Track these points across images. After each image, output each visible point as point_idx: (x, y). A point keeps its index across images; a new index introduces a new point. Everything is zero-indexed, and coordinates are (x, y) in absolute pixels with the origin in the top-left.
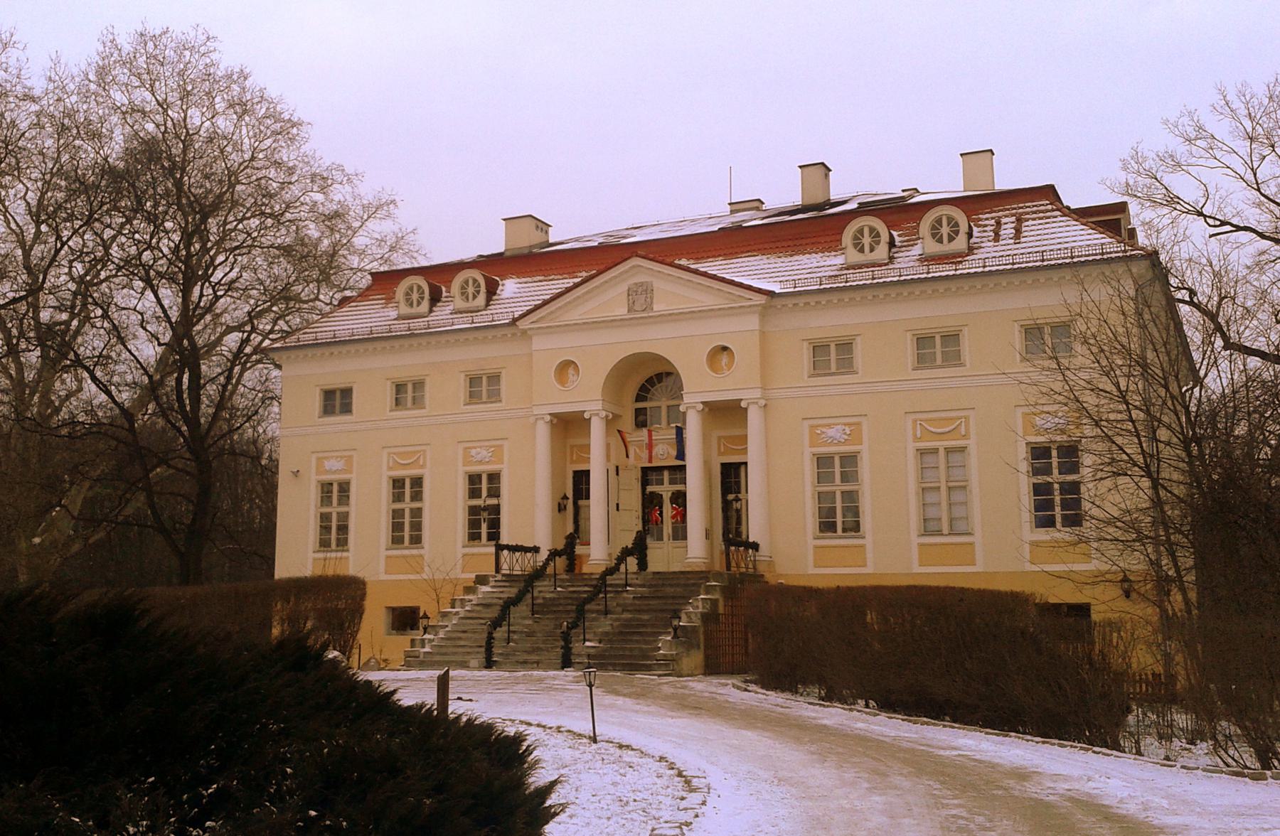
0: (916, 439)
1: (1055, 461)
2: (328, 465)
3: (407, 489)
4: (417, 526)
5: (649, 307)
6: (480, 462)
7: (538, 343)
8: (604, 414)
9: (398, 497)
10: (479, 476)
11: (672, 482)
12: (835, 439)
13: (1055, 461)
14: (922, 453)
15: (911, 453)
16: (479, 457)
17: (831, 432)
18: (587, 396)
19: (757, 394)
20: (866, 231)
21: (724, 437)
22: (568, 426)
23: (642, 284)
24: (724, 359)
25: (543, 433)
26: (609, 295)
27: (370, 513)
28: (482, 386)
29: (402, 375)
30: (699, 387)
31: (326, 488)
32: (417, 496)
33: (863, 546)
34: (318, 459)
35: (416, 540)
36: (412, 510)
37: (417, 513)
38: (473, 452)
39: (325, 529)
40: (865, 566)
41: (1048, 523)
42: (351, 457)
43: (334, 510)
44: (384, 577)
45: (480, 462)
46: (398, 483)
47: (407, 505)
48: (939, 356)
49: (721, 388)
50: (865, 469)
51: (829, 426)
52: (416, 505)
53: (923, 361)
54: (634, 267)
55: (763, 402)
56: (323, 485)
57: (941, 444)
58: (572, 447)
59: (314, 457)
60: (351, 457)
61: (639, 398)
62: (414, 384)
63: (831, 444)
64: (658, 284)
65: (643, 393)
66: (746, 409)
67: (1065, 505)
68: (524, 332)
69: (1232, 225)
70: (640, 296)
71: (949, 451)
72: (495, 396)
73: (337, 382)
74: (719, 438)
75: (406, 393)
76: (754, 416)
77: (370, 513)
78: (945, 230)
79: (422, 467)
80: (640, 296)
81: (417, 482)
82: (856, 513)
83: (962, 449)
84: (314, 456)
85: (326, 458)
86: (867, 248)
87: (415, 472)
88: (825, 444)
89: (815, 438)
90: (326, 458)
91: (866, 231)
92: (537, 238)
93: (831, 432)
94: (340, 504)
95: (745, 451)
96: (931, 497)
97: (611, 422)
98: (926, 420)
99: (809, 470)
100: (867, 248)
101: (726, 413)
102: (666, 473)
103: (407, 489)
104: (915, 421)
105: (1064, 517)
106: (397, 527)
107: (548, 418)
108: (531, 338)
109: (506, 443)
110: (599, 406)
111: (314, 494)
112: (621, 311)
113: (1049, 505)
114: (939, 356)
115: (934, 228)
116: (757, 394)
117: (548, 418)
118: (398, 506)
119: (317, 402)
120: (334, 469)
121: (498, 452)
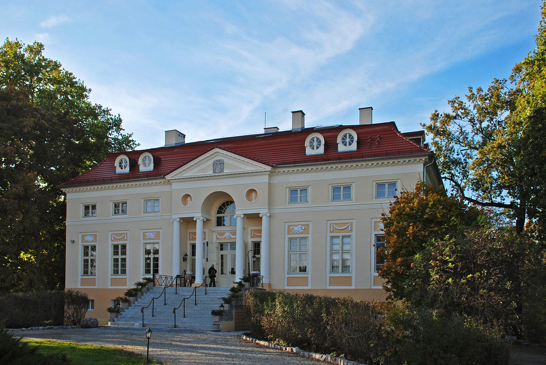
0: (112, 241)
2: (86, 238)
3: (120, 249)
4: (124, 266)
5: (222, 171)
7: (175, 186)
8: (202, 218)
9: (116, 253)
10: (88, 247)
14: (332, 237)
16: (149, 237)
19: (266, 211)
20: (315, 139)
21: (254, 230)
22: (188, 222)
24: (253, 195)
25: (176, 226)
26: (202, 166)
27: (104, 258)
32: (124, 253)
34: (144, 233)
36: (88, 260)
37: (124, 260)
38: (147, 234)
39: (116, 266)
42: (96, 235)
43: (120, 257)
44: (110, 287)
46: (116, 247)
48: (299, 198)
52: (123, 257)
55: (268, 215)
56: (114, 246)
57: (341, 234)
58: (190, 233)
60: (96, 235)
61: (219, 212)
62: (92, 206)
63: (296, 234)
64: (226, 161)
65: (221, 210)
66: (262, 217)
68: (169, 181)
70: (219, 165)
71: (301, 238)
72: (348, 197)
73: (90, 202)
74: (251, 230)
75: (119, 207)
76: (265, 220)
77: (104, 258)
78: (348, 140)
79: (126, 240)
81: (124, 247)
83: (306, 238)
86: (315, 148)
88: (294, 233)
89: (290, 231)
91: (315, 139)
92: (180, 141)
93: (296, 228)
94: (122, 254)
95: (261, 236)
97: (206, 222)
98: (335, 224)
100: (315, 148)
103: (120, 249)
104: (331, 224)
107: (179, 219)
108: (172, 183)
109: (354, 221)
110: (200, 215)
112: (210, 173)
114: (299, 198)
115: (343, 139)
117: (179, 219)
118: (116, 257)
120: (89, 240)
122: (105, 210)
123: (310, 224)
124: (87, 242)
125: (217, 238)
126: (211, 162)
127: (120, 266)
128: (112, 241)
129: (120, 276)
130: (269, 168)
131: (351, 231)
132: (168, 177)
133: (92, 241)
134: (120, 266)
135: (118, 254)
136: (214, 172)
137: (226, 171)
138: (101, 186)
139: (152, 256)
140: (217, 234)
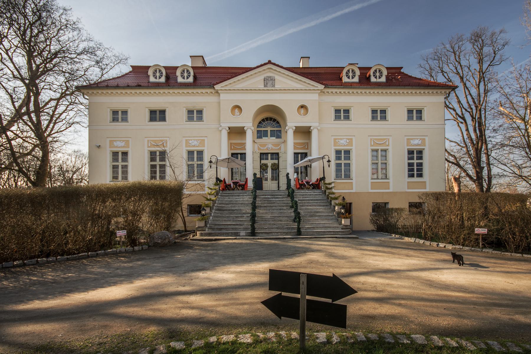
0: (148, 147)
1: (415, 155)
5: (274, 86)
6: (194, 146)
11: (272, 159)
12: (415, 144)
13: (415, 155)
15: (370, 151)
16: (193, 144)
17: (342, 142)
18: (247, 121)
22: (237, 132)
23: (270, 77)
25: (225, 134)
27: (398, 163)
28: (195, 114)
29: (116, 107)
30: (293, 120)
31: (115, 154)
32: (421, 158)
33: (352, 183)
34: (111, 141)
35: (420, 175)
38: (190, 142)
40: (352, 189)
41: (412, 176)
45: (194, 146)
47: (343, 162)
49: (303, 121)
50: (353, 155)
51: (341, 139)
53: (374, 118)
54: (268, 68)
57: (380, 148)
59: (108, 140)
60: (128, 141)
64: (277, 77)
67: (418, 170)
69: (480, 82)
70: (269, 81)
75: (158, 115)
79: (388, 145)
80: (269, 81)
82: (113, 172)
84: (108, 140)
85: (115, 141)
87: (199, 149)
88: (339, 146)
90: (115, 141)
93: (342, 142)
96: (384, 166)
99: (185, 156)
101: (304, 132)
102: (239, 155)
105: (417, 174)
106: (411, 170)
107: (228, 129)
110: (251, 124)
111: (109, 157)
112: (262, 86)
113: (412, 170)
116: (317, 124)
119: (184, 115)
120: (120, 147)
121: (202, 142)
122: (176, 115)
123: (353, 138)
124: (117, 147)
125: (259, 149)
126: (262, 77)
127: (415, 170)
128: (148, 147)
129: (416, 179)
130: (321, 87)
131: (388, 145)
132: (216, 87)
133: (123, 147)
134: (415, 170)
135: (193, 160)
136: (265, 86)
137: (277, 86)
138: (102, 91)
139: (269, 162)
140: (269, 144)
